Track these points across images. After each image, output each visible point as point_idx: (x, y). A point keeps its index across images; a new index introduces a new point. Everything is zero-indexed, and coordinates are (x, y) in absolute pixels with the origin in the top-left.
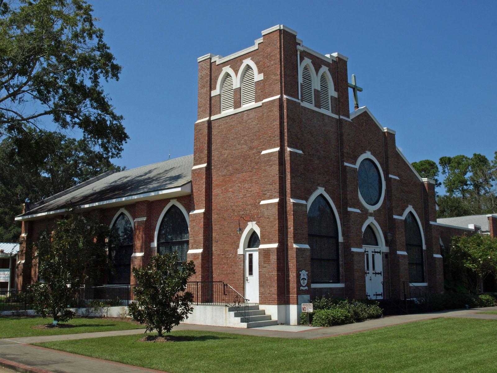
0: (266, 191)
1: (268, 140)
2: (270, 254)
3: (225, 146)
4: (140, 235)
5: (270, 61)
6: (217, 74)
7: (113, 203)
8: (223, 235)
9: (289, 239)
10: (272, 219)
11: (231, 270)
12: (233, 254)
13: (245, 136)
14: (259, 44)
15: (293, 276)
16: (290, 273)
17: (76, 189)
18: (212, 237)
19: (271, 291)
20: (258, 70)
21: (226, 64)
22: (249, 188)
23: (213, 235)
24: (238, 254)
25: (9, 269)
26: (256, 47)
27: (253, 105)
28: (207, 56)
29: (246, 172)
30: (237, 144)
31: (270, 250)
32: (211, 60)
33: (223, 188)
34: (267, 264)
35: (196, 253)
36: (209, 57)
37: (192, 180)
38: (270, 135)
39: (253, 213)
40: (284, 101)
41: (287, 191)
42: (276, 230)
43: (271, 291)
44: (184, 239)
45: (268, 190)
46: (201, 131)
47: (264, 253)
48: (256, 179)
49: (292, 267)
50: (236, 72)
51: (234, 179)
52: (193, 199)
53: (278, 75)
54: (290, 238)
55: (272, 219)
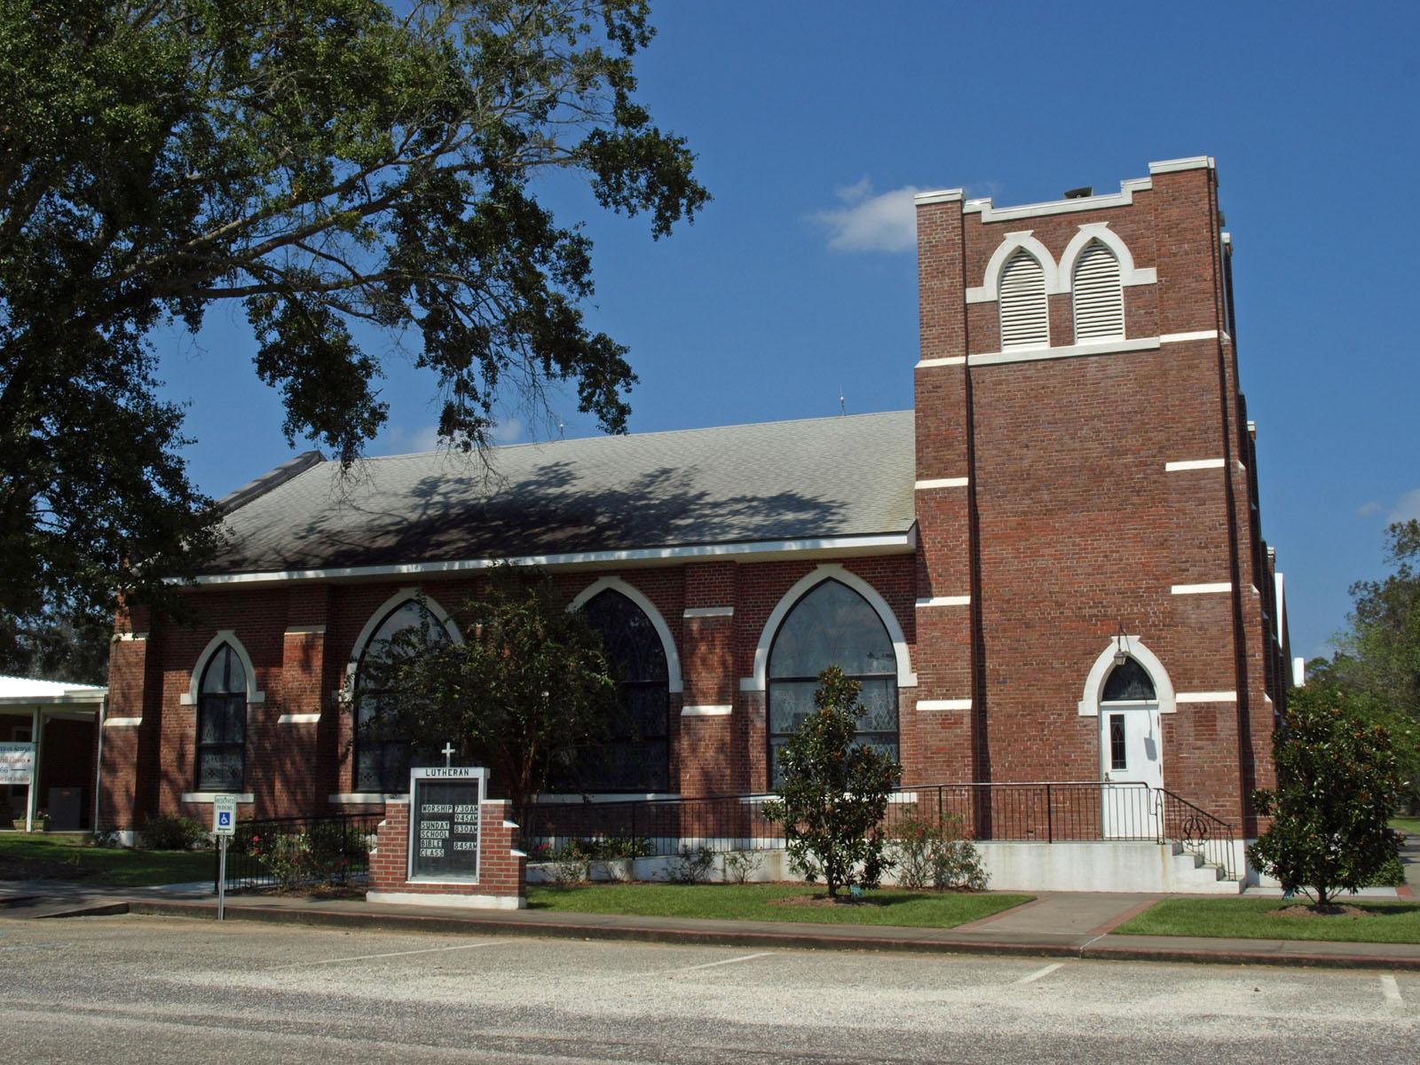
0: (1187, 562)
1: (1182, 437)
2: (1215, 717)
3: (1024, 438)
4: (715, 659)
5: (1181, 242)
6: (984, 245)
7: (620, 561)
8: (1026, 665)
9: (1250, 681)
10: (1213, 631)
11: (1056, 757)
12: (1060, 715)
13: (1093, 418)
14: (1134, 192)
15: (1264, 770)
16: (1257, 763)
17: (241, 500)
18: (984, 670)
19: (1222, 806)
20: (1134, 259)
21: (1015, 224)
22: (1112, 552)
23: (987, 664)
24: (1080, 714)
25: (31, 745)
26: (1124, 198)
27: (1117, 342)
28: (956, 193)
29: (1100, 511)
30: (1067, 437)
31: (1215, 707)
32: (962, 207)
33: (1022, 546)
34: (1208, 740)
35: (950, 711)
36: (958, 197)
37: (918, 517)
38: (1189, 425)
39: (1128, 614)
40: (1226, 346)
41: (1240, 565)
42: (1230, 659)
43: (1222, 806)
44: (870, 671)
45: (1195, 561)
46: (939, 390)
47: (1195, 713)
48: (1136, 529)
49: (1263, 749)
50: (1057, 254)
51: (1057, 525)
52: (926, 567)
53: (1205, 280)
54: (1255, 678)
55: (1213, 631)
